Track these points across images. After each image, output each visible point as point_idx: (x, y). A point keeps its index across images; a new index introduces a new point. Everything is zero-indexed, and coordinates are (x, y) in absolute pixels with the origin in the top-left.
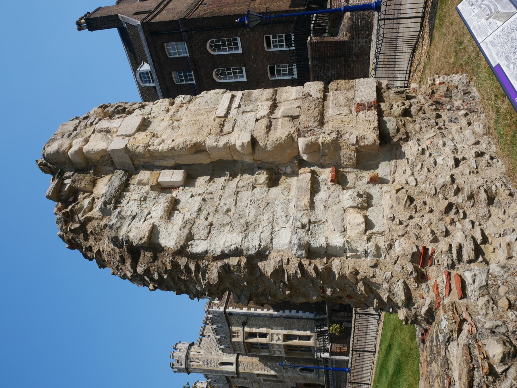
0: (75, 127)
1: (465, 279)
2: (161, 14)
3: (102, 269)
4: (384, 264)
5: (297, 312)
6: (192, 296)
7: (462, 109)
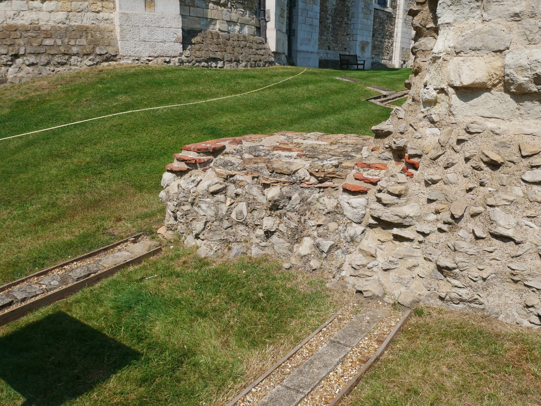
1: (357, 197)
4: (415, 111)
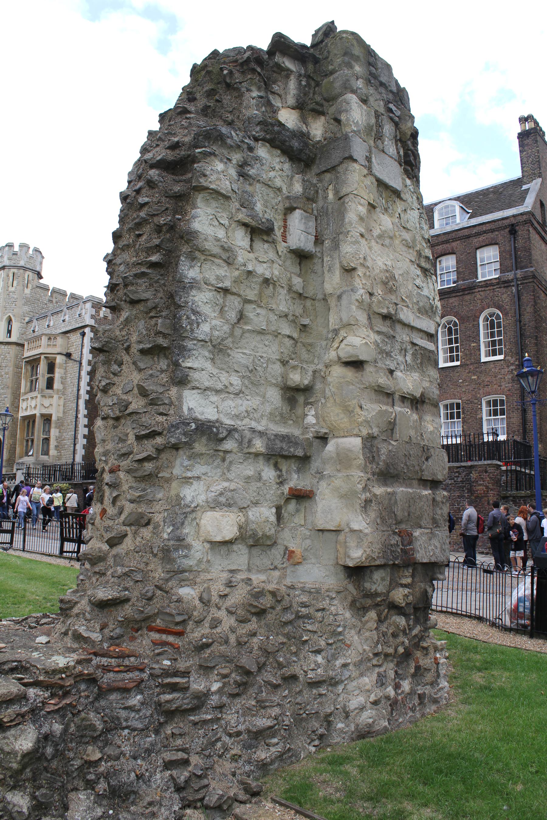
0: (385, 84)
3: (158, 119)
5: (85, 437)
6: (109, 258)
7: (396, 692)
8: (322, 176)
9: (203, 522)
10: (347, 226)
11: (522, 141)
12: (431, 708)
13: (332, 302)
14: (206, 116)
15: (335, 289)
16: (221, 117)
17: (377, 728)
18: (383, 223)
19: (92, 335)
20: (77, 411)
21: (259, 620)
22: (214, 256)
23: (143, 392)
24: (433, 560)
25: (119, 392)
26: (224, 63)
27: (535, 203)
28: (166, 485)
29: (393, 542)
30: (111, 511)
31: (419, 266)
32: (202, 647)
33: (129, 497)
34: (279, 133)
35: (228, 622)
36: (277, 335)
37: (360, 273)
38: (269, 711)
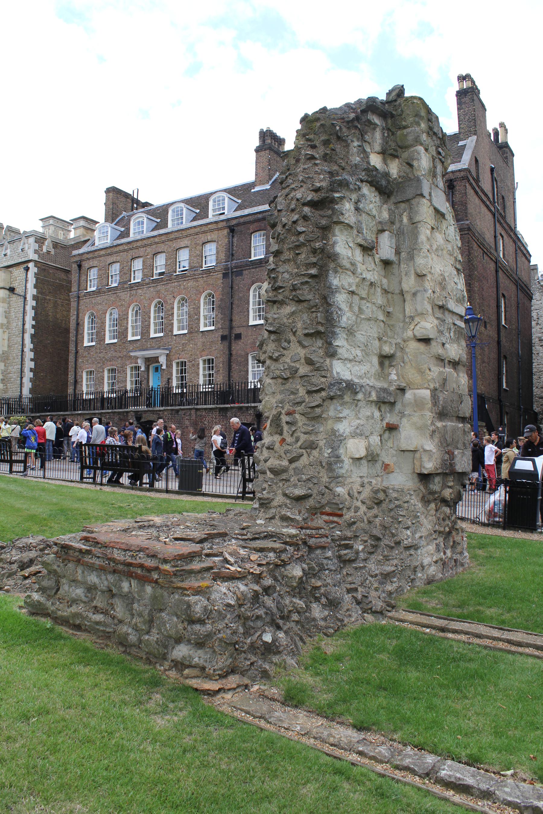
2: (475, 197)
5: (31, 370)
8: (399, 205)
9: (348, 446)
10: (420, 245)
11: (460, 99)
12: (460, 569)
13: (408, 297)
14: (326, 161)
15: (410, 288)
16: (336, 162)
17: (437, 578)
18: (438, 240)
19: (36, 270)
20: (23, 345)
21: (378, 508)
22: (347, 269)
23: (309, 362)
24: (464, 470)
25: (288, 360)
26: (334, 119)
27: (471, 160)
28: (324, 423)
29: (446, 458)
30: (289, 440)
31: (456, 268)
32: (351, 524)
33: (303, 430)
34: (376, 176)
35: (363, 508)
36: (376, 320)
37: (428, 278)
38: (391, 562)
